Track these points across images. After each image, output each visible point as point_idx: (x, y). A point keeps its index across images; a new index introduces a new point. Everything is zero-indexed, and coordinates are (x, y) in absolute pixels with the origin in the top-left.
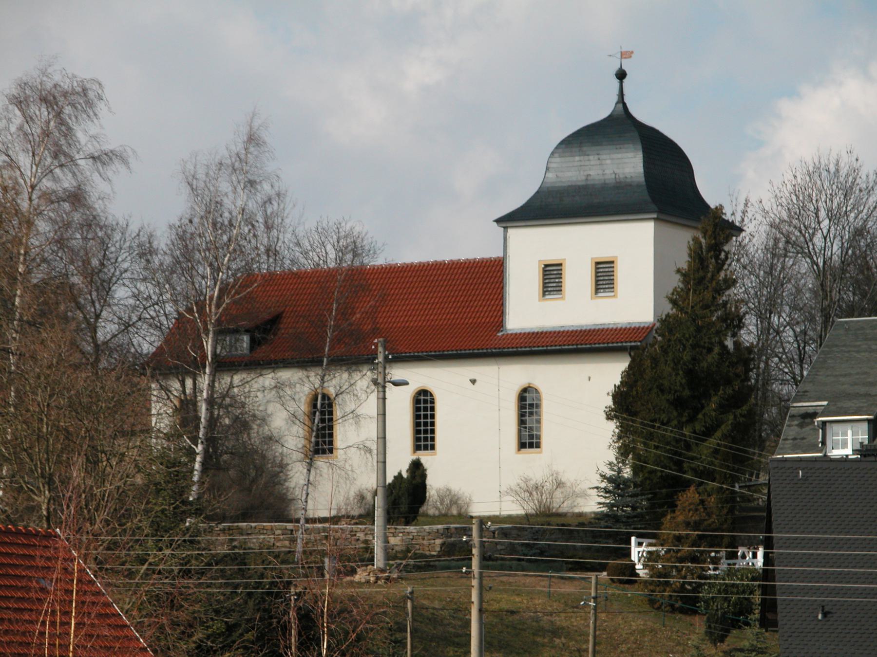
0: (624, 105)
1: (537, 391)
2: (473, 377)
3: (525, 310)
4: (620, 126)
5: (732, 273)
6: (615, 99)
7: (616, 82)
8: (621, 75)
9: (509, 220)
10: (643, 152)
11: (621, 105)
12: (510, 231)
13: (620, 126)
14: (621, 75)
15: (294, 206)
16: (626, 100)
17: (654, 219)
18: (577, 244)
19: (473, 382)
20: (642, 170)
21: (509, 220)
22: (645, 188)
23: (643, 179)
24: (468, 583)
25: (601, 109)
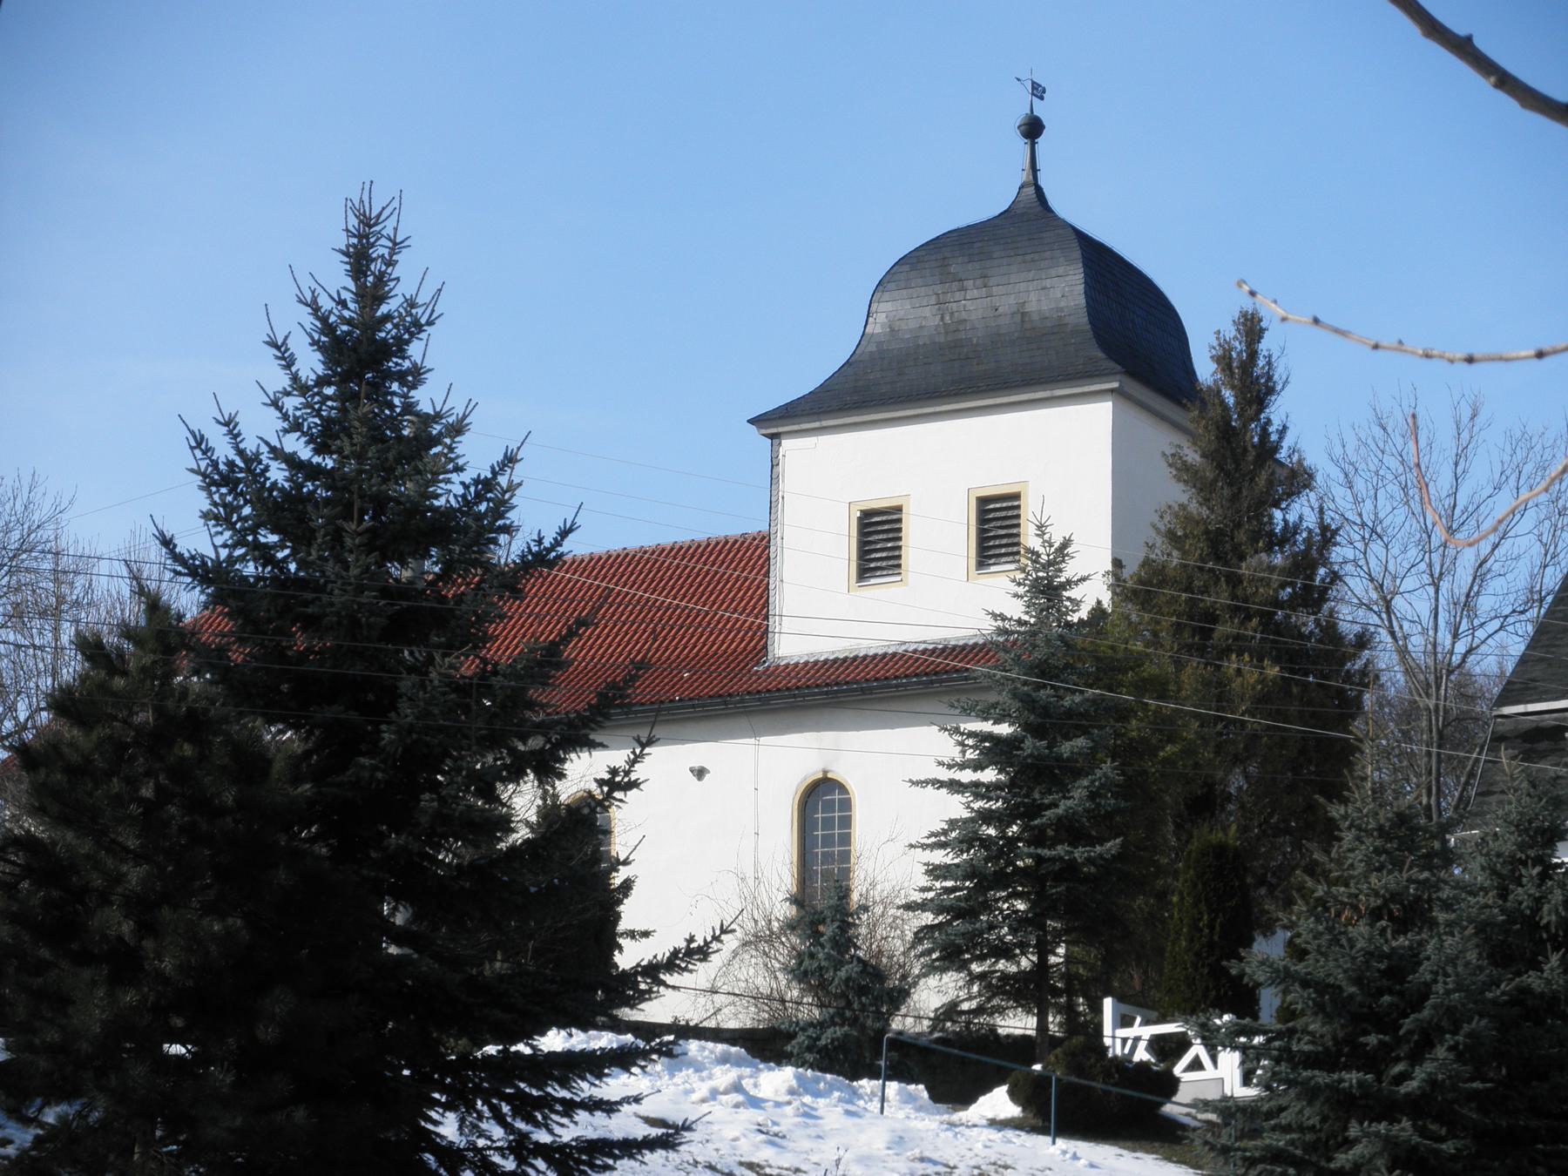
0: (1039, 191)
1: (842, 788)
2: (696, 765)
3: (817, 612)
4: (1030, 223)
5: (1226, 1163)
6: (1024, 176)
7: (1021, 146)
8: (1033, 129)
9: (780, 421)
10: (1085, 265)
11: (1031, 190)
12: (787, 444)
13: (1030, 223)
14: (1033, 129)
15: (819, 1137)
16: (1042, 183)
17: (1112, 391)
18: (935, 463)
19: (700, 773)
20: (1082, 301)
21: (780, 421)
22: (1091, 335)
23: (1086, 319)
24: (71, 733)
25: (993, 196)
